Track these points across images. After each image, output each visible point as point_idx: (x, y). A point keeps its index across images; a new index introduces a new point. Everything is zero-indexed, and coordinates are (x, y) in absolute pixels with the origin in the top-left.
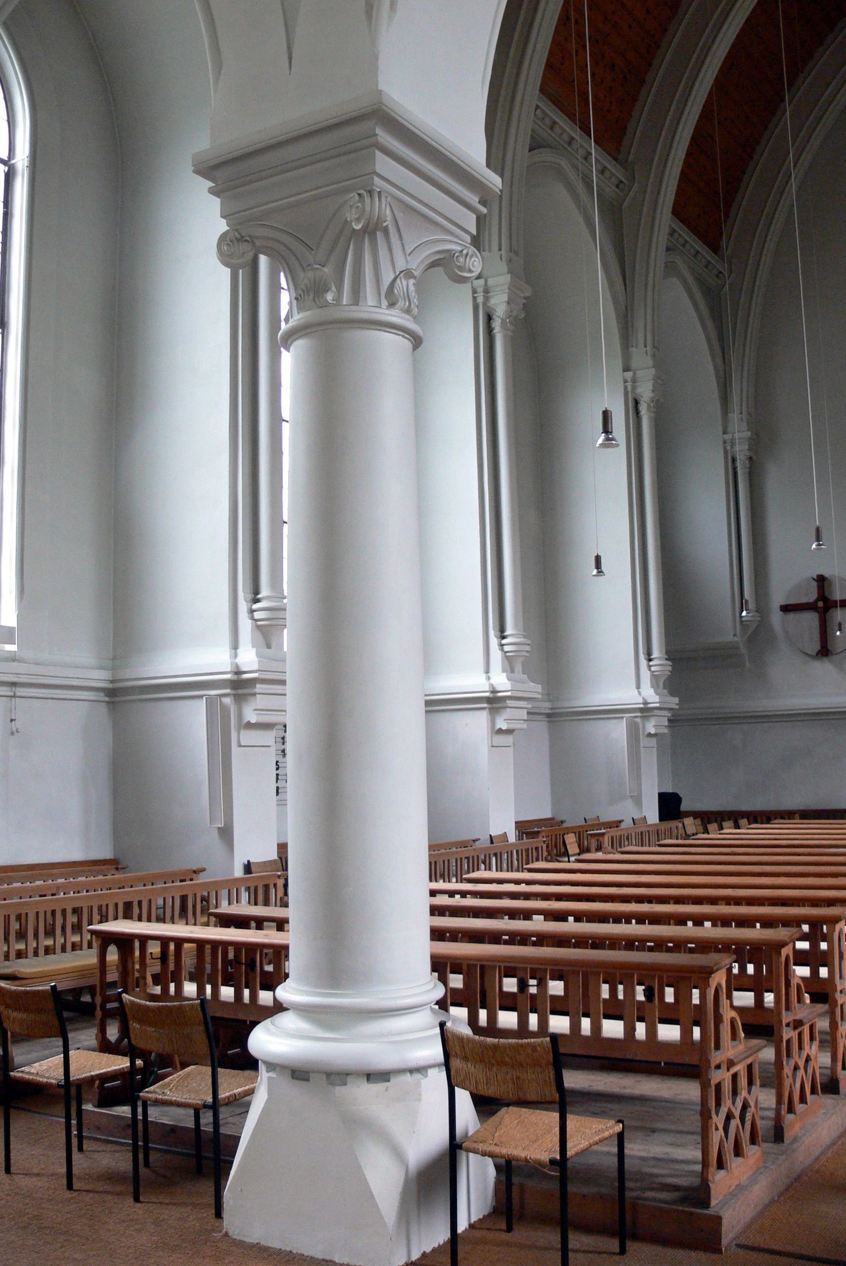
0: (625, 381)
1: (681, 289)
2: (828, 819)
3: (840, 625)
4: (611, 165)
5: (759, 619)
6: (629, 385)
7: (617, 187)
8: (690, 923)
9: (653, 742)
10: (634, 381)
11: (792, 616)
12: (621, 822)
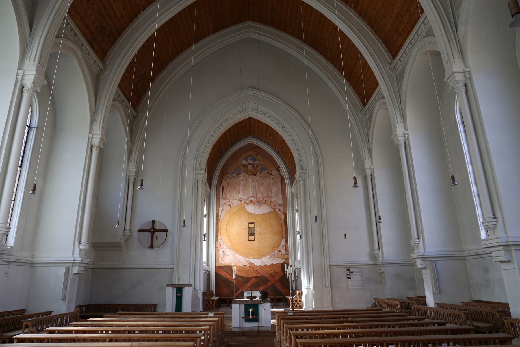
0: (89, 138)
1: (119, 116)
2: (128, 311)
3: (157, 237)
4: (133, 110)
6: (90, 139)
9: (77, 277)
10: (92, 138)
11: (142, 233)
12: (51, 312)
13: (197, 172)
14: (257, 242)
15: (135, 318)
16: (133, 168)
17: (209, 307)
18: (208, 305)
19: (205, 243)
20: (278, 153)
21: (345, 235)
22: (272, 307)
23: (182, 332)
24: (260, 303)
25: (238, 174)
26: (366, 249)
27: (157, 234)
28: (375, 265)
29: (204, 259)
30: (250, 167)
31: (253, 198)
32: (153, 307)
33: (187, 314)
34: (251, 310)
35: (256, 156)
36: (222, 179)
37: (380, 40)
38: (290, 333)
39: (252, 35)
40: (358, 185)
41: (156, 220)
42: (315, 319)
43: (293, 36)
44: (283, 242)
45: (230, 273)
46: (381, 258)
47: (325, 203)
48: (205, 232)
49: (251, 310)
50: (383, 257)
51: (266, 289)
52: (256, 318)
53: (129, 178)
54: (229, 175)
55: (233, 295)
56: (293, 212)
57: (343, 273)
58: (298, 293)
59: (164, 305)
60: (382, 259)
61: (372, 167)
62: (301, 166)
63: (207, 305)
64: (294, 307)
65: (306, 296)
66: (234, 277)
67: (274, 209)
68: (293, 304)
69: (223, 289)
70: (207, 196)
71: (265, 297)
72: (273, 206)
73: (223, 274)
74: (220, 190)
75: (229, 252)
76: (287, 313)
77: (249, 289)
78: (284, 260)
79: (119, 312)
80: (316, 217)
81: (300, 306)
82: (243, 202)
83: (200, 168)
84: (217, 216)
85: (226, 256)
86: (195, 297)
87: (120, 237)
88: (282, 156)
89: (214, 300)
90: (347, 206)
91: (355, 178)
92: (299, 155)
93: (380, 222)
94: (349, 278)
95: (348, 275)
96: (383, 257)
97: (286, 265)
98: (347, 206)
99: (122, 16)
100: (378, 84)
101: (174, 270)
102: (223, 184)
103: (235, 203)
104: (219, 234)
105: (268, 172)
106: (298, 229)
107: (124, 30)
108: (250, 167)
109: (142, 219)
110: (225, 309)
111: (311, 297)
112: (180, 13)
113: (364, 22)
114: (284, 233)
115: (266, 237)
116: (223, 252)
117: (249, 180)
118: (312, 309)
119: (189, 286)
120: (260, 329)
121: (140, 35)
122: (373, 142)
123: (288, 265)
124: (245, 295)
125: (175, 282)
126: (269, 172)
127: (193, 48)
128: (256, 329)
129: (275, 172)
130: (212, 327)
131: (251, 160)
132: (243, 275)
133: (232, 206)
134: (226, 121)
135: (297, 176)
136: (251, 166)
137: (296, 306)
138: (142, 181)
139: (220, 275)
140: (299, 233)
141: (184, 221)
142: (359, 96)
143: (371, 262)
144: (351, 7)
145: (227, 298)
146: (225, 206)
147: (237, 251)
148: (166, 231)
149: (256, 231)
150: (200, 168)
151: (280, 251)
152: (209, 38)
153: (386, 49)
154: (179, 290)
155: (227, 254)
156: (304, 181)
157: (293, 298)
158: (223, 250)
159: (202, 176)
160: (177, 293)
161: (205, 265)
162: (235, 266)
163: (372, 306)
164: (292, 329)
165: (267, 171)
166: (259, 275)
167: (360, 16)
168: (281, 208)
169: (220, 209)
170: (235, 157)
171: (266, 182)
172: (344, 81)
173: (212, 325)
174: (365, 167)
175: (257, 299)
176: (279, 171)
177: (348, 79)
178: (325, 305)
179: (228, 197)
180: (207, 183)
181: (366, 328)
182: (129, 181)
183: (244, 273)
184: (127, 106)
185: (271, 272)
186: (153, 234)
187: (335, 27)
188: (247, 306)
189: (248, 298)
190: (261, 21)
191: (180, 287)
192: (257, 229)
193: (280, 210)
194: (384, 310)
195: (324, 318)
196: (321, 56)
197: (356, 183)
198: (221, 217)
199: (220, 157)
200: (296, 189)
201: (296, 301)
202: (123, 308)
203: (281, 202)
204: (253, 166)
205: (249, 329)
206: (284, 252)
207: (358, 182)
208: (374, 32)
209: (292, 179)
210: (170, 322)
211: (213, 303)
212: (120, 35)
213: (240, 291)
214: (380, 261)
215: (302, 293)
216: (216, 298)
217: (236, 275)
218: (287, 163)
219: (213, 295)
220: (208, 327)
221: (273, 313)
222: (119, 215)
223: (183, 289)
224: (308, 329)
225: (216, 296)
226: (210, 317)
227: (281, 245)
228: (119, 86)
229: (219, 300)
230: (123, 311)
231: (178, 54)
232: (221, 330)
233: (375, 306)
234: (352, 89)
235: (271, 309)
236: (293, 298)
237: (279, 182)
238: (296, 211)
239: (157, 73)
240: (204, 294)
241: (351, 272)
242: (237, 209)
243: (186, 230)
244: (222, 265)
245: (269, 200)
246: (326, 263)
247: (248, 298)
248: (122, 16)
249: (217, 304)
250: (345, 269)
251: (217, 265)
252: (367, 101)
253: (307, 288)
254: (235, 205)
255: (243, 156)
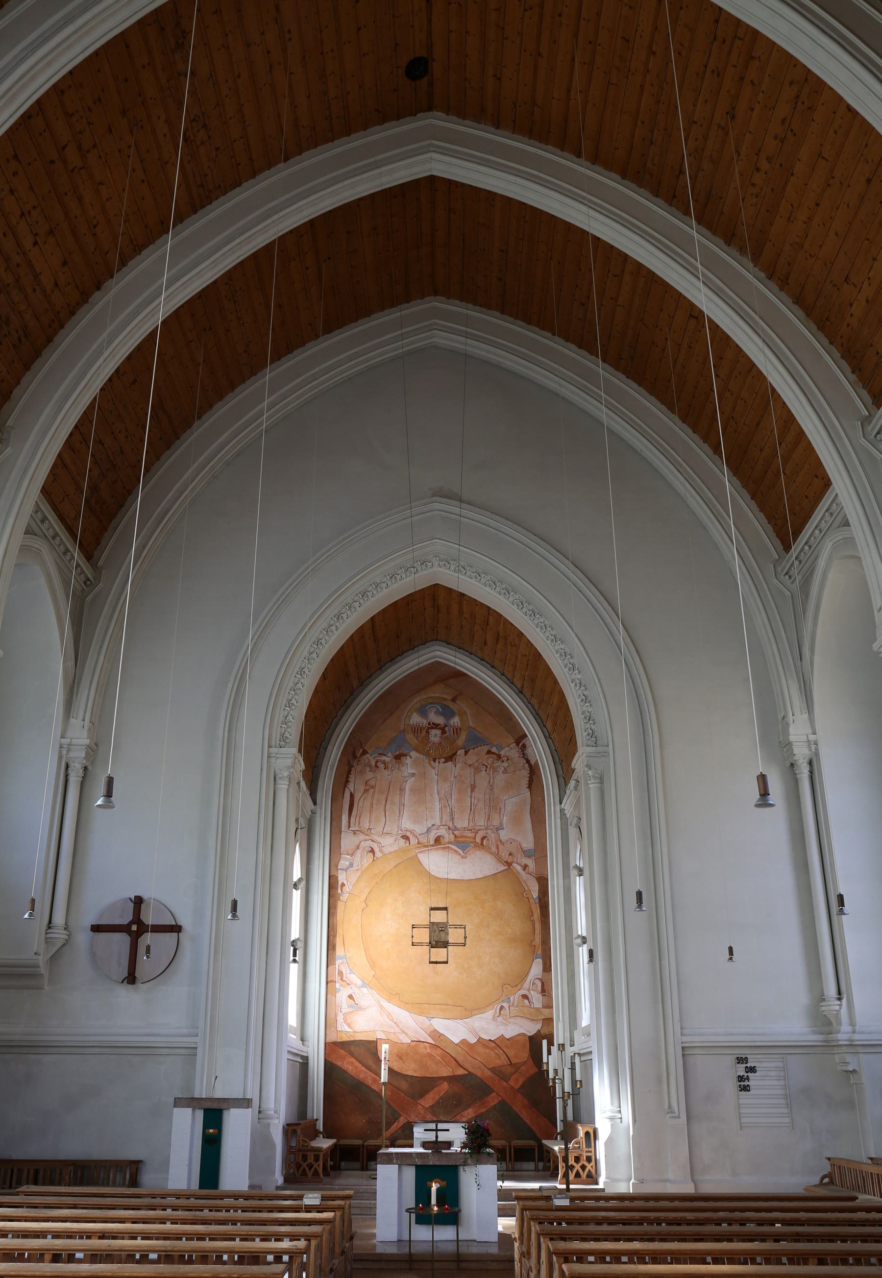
1: (42, 581)
2: (51, 1183)
3: (148, 948)
4: (83, 563)
5: (66, 937)
7: (85, 583)
8: (239, 1224)
11: (102, 936)
13: (273, 750)
14: (458, 967)
15: (75, 1207)
16: (80, 735)
17: (304, 1173)
18: (302, 1167)
19: (294, 970)
20: (520, 692)
21: (731, 949)
22: (502, 1177)
23: (219, 1260)
24: (465, 1164)
25: (398, 757)
26: (799, 996)
27: (148, 938)
28: (829, 1046)
29: (292, 1019)
30: (435, 736)
31: (442, 832)
32: (130, 1172)
33: (236, 1196)
34: (434, 1187)
35: (454, 700)
36: (349, 772)
37: (833, 349)
38: (562, 1271)
39: (442, 339)
40: (771, 799)
41: (145, 896)
42: (640, 1222)
43: (567, 340)
44: (537, 968)
45: (370, 1062)
46: (845, 1027)
47: (665, 850)
48: (295, 933)
49: (434, 1187)
50: (852, 1023)
51: (478, 1117)
52: (450, 1213)
53: (67, 767)
54: (370, 759)
55: (379, 1135)
56: (566, 876)
57: (725, 1072)
58: (581, 1134)
59: (165, 1165)
60: (849, 1029)
61: (812, 737)
62: (592, 735)
63: (298, 1166)
64: (572, 1176)
65: (609, 1142)
66: (384, 1077)
67: (509, 864)
68: (569, 1168)
69: (347, 1118)
70: (303, 822)
71: (478, 1143)
72: (505, 855)
73: (350, 1065)
74: (344, 806)
75: (368, 998)
76: (549, 1198)
77: (429, 1117)
78: (538, 1026)
79: (24, 1188)
80: (639, 894)
81: (589, 1175)
82: (413, 841)
83: (283, 738)
84: (333, 885)
85: (361, 1009)
86: (259, 1140)
87: (34, 948)
88: (534, 701)
89: (319, 1150)
90: (735, 858)
91: (762, 779)
92: (586, 699)
93: (841, 912)
94: (746, 1089)
95: (741, 1078)
96: (852, 1023)
97: (545, 1042)
98: (735, 858)
99: (56, 285)
100: (827, 483)
101: (199, 1052)
102: (351, 786)
103: (390, 844)
104: (339, 941)
105: (489, 752)
106: (582, 927)
107: (62, 327)
108: (435, 736)
109: (105, 893)
110: (352, 1181)
111: (625, 1147)
112: (229, 276)
113: (783, 294)
114: (538, 940)
115: (485, 950)
116: (351, 997)
117: (432, 773)
118: (626, 1187)
119: (245, 1103)
120: (463, 1249)
121: (110, 342)
122: (817, 658)
123: (551, 1043)
124: (416, 1135)
125: (201, 1092)
126: (494, 750)
127: (268, 375)
128: (452, 1248)
129: (511, 751)
130: (314, 1243)
131: (437, 713)
132: (410, 1069)
133: (378, 854)
134: (364, 594)
135: (579, 763)
136: (439, 732)
137: (578, 1175)
138: (110, 781)
139: (340, 1069)
140: (584, 940)
141: (235, 904)
142: (770, 518)
143: (815, 1038)
144: (742, 250)
145: (359, 1142)
146: (358, 853)
147: (394, 996)
148: (176, 929)
149: (454, 936)
150: (283, 738)
151: (525, 997)
152: (313, 349)
153: (853, 377)
154: (213, 1116)
155: (363, 1003)
156: (601, 780)
157: (567, 1149)
158: (350, 992)
159: (289, 762)
160: (206, 1126)
161: (293, 1037)
162: (387, 1041)
163: (821, 1184)
164: (566, 1257)
165: (486, 748)
166: (461, 1072)
167: (770, 277)
168: (530, 863)
169: (343, 863)
170: (393, 700)
171: (483, 780)
172: (726, 478)
173: (315, 1236)
174: (792, 738)
175: (456, 1148)
176: (524, 746)
177: (736, 469)
178: (670, 1176)
179: (366, 825)
180: (303, 784)
181: (806, 1262)
182: (67, 776)
183: (413, 1065)
184: (67, 551)
185: (498, 1062)
186: (135, 938)
187: (695, 315)
188: (425, 1173)
189: (425, 1145)
190: (469, 294)
191: (215, 1106)
192: (456, 927)
193: (525, 867)
194: (864, 1198)
195: (670, 1223)
196: (653, 399)
197: (764, 793)
198: (346, 889)
199: (345, 704)
200: (577, 806)
201: (577, 1159)
202: (37, 1171)
203: (528, 843)
204: (444, 732)
205: (427, 1248)
206: (537, 1000)
207: (771, 791)
208: (814, 327)
209: (565, 773)
210: (184, 1222)
211: (317, 1159)
212: (49, 340)
213: (402, 1120)
214: (843, 1035)
215: (595, 1131)
216: (325, 1144)
217: (391, 1071)
218: (549, 725)
219: (315, 1134)
220: (302, 1244)
221: (503, 1195)
222: (35, 882)
223: (225, 1113)
224: (616, 1257)
225: (328, 1135)
226: (309, 1209)
227: (530, 977)
228: (45, 491)
229: (334, 1149)
230: (36, 1183)
231: (221, 396)
232: (343, 1252)
233: (832, 1182)
234: (748, 497)
235: (500, 1183)
236: (567, 1149)
237: (525, 782)
238: (575, 872)
239: (155, 457)
240: (290, 1130)
241: (752, 1070)
242: (393, 864)
243: (239, 930)
244: (345, 1038)
245: (492, 836)
246: (670, 1040)
247: (425, 1145)
248: (56, 285)
249: (330, 1163)
250: (731, 1060)
251: (332, 1038)
252: (797, 533)
253: (612, 1119)
254: (387, 850)
255: (413, 699)
